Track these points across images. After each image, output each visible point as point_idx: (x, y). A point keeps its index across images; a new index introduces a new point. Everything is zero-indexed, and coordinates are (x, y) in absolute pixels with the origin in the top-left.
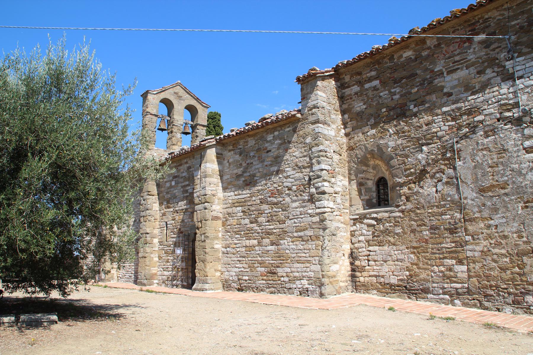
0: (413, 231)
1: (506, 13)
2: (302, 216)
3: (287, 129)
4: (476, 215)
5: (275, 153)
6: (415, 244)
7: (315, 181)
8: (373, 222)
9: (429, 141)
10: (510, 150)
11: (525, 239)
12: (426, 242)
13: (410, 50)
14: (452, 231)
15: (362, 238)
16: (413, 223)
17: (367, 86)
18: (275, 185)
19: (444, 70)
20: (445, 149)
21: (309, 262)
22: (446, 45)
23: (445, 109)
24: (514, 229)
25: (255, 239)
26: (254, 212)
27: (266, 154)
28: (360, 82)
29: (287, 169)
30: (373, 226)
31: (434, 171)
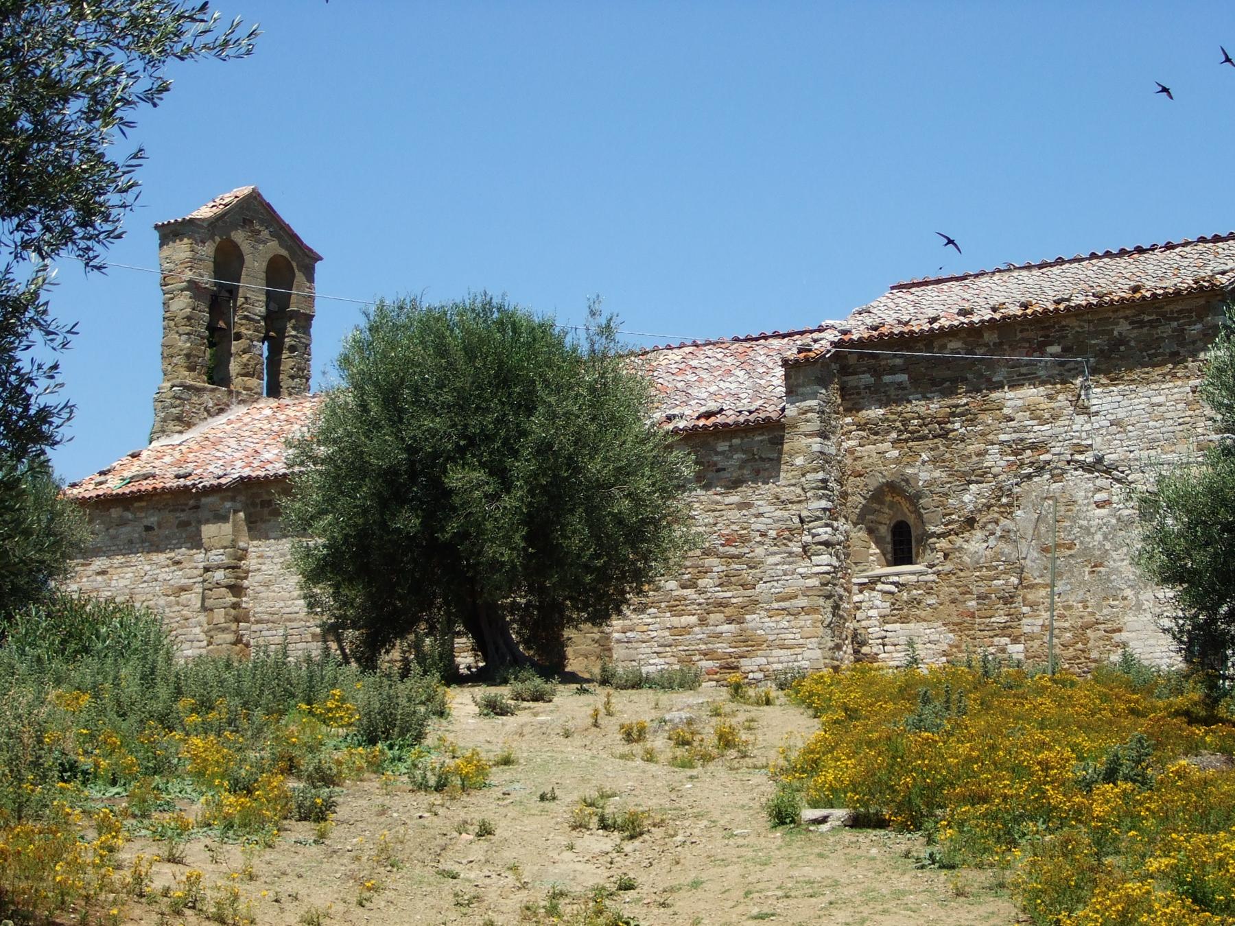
0: (953, 601)
1: (1086, 326)
2: (788, 577)
3: (760, 438)
4: (1036, 581)
5: (735, 475)
6: (956, 620)
7: (811, 525)
8: (893, 588)
9: (982, 475)
10: (1080, 502)
11: (1090, 610)
12: (973, 616)
13: (959, 340)
14: (1008, 600)
15: (872, 613)
16: (953, 589)
17: (887, 379)
18: (734, 527)
19: (1005, 382)
20: (1001, 491)
21: (800, 646)
22: (1010, 346)
23: (1003, 437)
24: (1079, 598)
25: (694, 615)
26: (690, 570)
27: (714, 474)
28: (875, 371)
29: (759, 503)
30: (892, 593)
31: (984, 520)
